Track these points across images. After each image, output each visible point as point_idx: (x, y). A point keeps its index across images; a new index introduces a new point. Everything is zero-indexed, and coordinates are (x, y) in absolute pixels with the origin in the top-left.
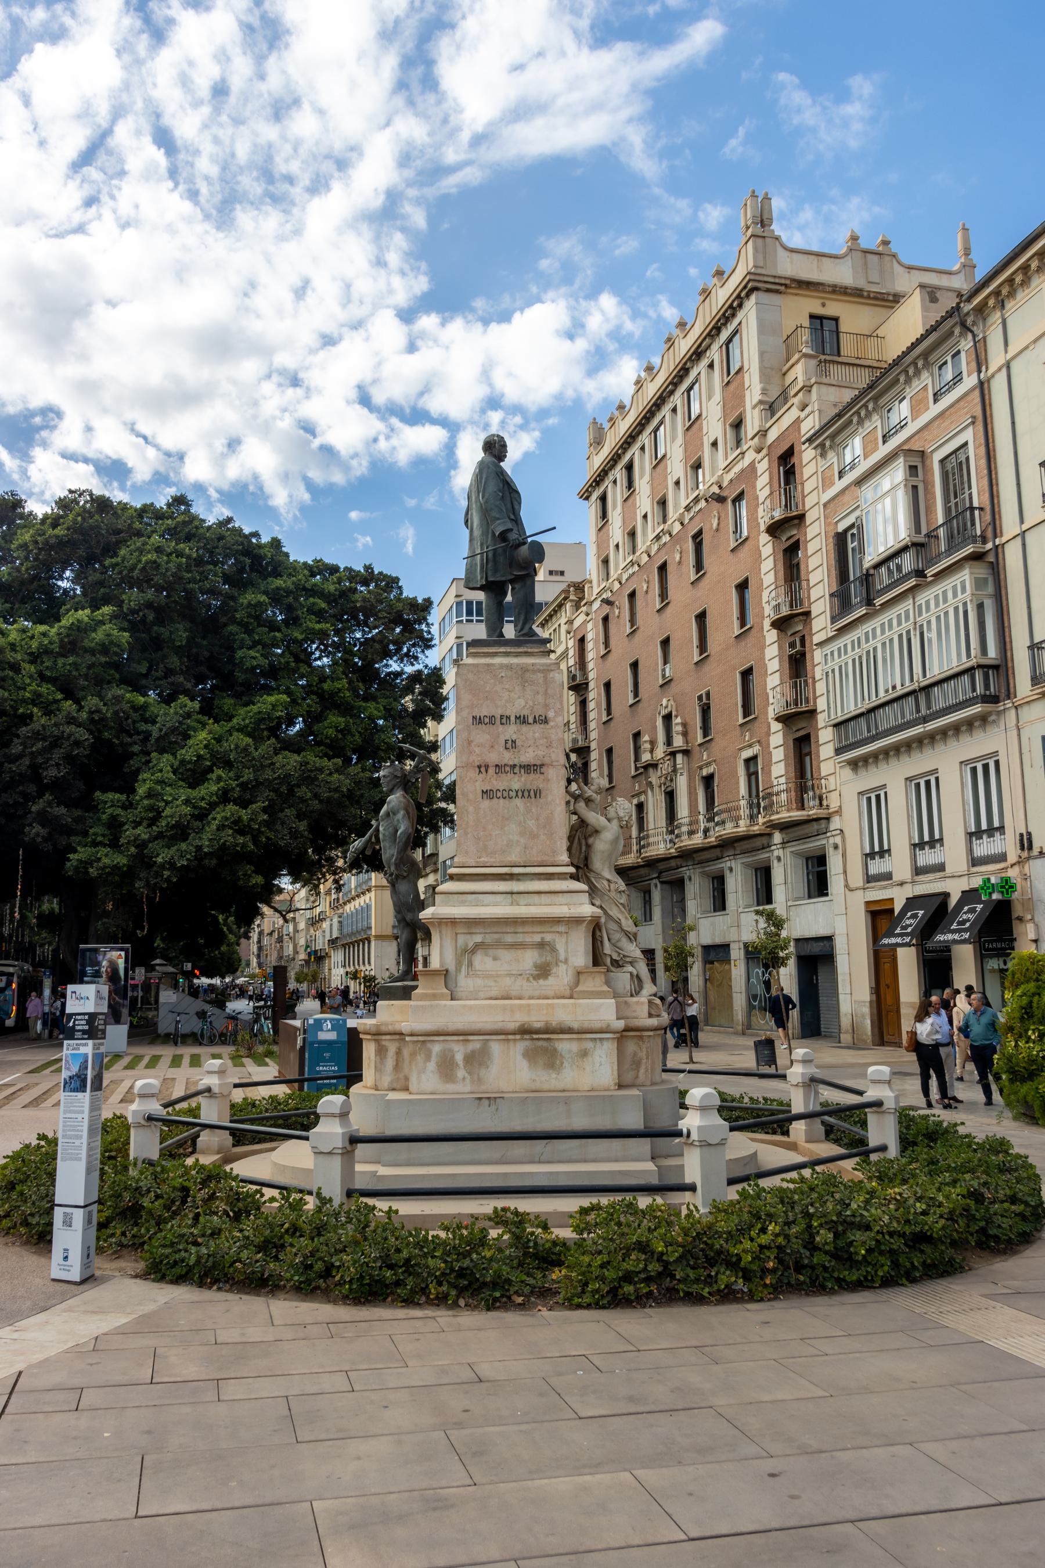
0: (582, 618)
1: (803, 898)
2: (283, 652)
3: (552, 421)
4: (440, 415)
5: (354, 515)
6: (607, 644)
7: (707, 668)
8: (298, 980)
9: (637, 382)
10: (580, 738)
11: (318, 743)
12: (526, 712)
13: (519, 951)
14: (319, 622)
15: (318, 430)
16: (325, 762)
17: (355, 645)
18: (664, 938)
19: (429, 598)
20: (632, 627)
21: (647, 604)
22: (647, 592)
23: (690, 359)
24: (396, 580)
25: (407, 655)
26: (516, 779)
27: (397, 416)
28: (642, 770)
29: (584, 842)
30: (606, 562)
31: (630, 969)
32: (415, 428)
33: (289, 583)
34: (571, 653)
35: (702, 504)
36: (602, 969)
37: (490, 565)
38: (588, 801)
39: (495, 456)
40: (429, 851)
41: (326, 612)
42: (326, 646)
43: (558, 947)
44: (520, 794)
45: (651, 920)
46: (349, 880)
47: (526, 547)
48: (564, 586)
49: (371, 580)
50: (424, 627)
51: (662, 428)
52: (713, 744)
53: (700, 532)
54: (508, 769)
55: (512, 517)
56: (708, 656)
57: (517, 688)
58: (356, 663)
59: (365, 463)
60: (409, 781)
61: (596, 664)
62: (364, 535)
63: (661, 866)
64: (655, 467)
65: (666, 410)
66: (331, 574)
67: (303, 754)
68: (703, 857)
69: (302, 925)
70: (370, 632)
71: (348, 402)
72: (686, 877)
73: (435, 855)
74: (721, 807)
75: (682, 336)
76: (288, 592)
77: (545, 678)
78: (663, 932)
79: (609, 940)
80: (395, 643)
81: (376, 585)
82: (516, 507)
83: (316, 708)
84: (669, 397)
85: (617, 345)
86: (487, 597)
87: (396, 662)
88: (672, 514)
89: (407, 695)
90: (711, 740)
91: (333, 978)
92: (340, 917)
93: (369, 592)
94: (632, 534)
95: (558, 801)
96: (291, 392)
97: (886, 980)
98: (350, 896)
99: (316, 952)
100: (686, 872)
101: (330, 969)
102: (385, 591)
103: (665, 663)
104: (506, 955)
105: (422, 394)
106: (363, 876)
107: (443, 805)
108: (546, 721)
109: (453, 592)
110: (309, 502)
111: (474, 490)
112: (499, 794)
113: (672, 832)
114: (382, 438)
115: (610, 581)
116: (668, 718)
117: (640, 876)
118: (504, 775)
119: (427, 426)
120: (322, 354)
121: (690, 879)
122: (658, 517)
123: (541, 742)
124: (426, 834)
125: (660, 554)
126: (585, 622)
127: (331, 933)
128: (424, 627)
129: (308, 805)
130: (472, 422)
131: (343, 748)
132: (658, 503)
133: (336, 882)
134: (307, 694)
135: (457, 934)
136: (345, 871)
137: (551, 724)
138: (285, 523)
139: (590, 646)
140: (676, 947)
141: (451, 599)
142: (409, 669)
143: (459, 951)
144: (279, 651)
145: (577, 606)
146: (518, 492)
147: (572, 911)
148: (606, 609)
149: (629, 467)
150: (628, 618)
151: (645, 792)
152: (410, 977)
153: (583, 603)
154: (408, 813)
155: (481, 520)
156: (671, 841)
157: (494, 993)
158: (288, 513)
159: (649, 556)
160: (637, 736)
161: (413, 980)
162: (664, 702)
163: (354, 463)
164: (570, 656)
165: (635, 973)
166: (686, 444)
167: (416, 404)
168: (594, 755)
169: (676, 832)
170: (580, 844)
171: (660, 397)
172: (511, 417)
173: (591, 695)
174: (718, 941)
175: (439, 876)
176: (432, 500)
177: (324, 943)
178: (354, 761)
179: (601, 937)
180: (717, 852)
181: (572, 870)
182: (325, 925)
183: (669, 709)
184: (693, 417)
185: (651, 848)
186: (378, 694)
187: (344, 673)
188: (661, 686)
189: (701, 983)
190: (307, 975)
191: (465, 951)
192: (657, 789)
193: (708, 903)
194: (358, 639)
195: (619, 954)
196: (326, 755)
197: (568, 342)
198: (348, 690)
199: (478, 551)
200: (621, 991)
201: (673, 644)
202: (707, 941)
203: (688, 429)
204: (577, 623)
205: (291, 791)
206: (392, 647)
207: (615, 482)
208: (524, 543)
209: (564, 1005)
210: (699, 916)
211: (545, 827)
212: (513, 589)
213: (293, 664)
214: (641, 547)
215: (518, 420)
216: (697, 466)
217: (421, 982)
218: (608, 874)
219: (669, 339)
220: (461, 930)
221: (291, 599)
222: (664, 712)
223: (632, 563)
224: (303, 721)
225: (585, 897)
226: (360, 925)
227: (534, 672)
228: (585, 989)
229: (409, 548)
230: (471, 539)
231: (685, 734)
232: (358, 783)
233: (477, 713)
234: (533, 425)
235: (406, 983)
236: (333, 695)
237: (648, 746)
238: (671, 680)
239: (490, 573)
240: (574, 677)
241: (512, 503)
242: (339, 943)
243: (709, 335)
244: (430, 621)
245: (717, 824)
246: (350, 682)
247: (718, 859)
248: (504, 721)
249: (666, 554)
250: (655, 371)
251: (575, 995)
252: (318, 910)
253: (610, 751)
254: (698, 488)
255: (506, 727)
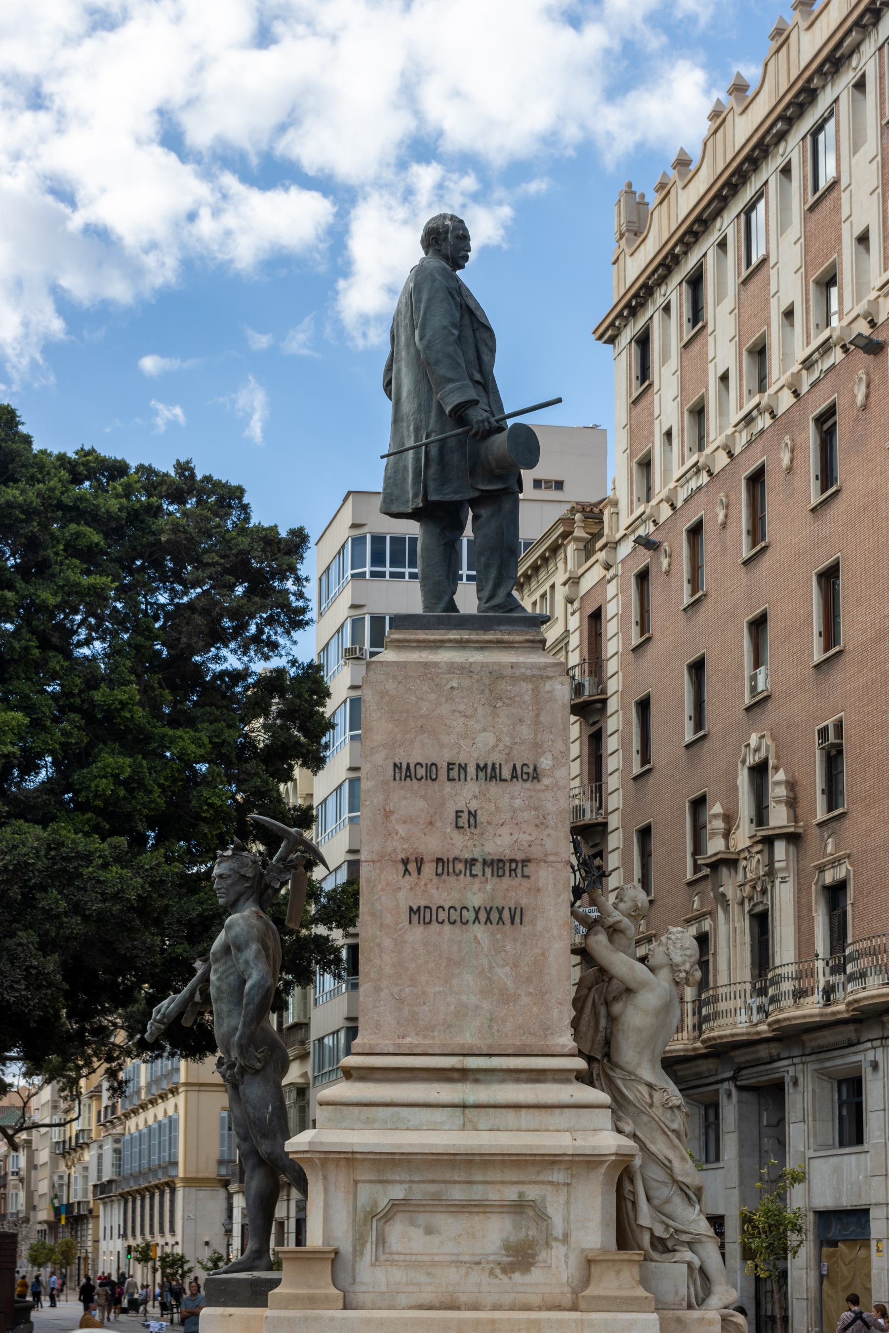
0: (596, 573)
1: (833, 1147)
2: (18, 629)
3: (536, 187)
4: (321, 169)
5: (149, 364)
6: (644, 624)
7: (838, 675)
8: (35, 1261)
9: (715, 115)
10: (587, 806)
11: (81, 807)
12: (496, 758)
13: (476, 1218)
14: (88, 572)
15: (80, 196)
16: (96, 843)
17: (156, 618)
18: (742, 1195)
19: (301, 529)
20: (694, 592)
21: (724, 550)
22: (724, 525)
23: (819, 70)
24: (239, 492)
25: (256, 639)
26: (476, 887)
27: (234, 171)
28: (706, 871)
29: (603, 1011)
30: (646, 464)
31: (688, 1255)
32: (271, 195)
33: (31, 494)
34: (574, 640)
35: (837, 355)
36: (634, 1255)
37: (432, 471)
38: (613, 931)
39: (446, 258)
40: (290, 1018)
41: (103, 552)
42: (100, 619)
43: (550, 1211)
44: (483, 916)
45: (717, 1159)
46: (137, 1069)
47: (501, 438)
48: (562, 511)
49: (190, 492)
50: (290, 585)
51: (761, 205)
52: (847, 822)
53: (831, 411)
54: (460, 866)
55: (478, 377)
56: (840, 652)
57: (480, 711)
58: (160, 652)
59: (171, 262)
60: (268, 886)
61: (623, 665)
62: (170, 402)
63: (741, 1056)
64: (745, 282)
65: (769, 170)
66: (112, 478)
67: (53, 826)
68: (822, 1042)
69: (43, 1156)
70: (185, 593)
71: (139, 142)
72: (787, 1079)
73: (302, 1026)
74: (857, 946)
75: (804, 25)
76: (29, 512)
77: (536, 691)
78: (741, 1183)
79: (648, 1199)
80: (234, 614)
81: (199, 502)
82: (486, 358)
83: (80, 738)
84: (777, 144)
85: (664, 39)
86: (426, 532)
87: (234, 651)
88: (777, 375)
89: (256, 716)
90: (843, 815)
91: (102, 1258)
92: (117, 1141)
93: (185, 514)
94: (698, 412)
95: (555, 931)
96: (28, 120)
97: (394, 1075)
98: (137, 1102)
99: (70, 1206)
100: (787, 1069)
101: (96, 1241)
102: (216, 514)
103: (757, 664)
104: (449, 1225)
105: (282, 128)
106: (164, 1064)
107: (320, 930)
108: (535, 776)
109: (347, 517)
110: (61, 336)
111: (404, 322)
112: (443, 915)
113: (762, 992)
114: (205, 213)
115: (654, 502)
116: (759, 771)
117: (699, 1076)
118: (452, 879)
119: (294, 191)
120: (89, 46)
121: (795, 1083)
122: (750, 381)
123: (526, 815)
124: (288, 985)
125: (751, 451)
126: (603, 582)
127: (100, 1171)
128: (290, 585)
129: (61, 926)
130: (380, 185)
131: (129, 816)
132: (750, 352)
133: (112, 1074)
134: (62, 710)
135: (356, 1182)
136: (128, 1053)
137: (546, 781)
138: (15, 376)
139: (611, 628)
140: (767, 1213)
141: (341, 533)
142: (260, 667)
143: (361, 1215)
144: (9, 626)
145: (588, 550)
146: (488, 329)
147: (580, 1142)
148: (645, 557)
149: (696, 281)
150: (686, 576)
151: (711, 914)
152: (263, 1263)
153: (599, 545)
154: (265, 947)
155: (417, 383)
156: (760, 1009)
157: (426, 1297)
158: (20, 355)
159: (730, 455)
160: (699, 804)
161: (270, 1268)
162: (754, 740)
163: (150, 261)
164: (571, 647)
165: (697, 1263)
166: (808, 239)
167: (272, 148)
168: (614, 841)
169: (771, 992)
170: (596, 1015)
171: (760, 145)
172: (455, 176)
173: (612, 724)
174: (846, 1202)
175: (309, 1067)
176: (301, 337)
177: (85, 1190)
178: (151, 842)
179: (634, 1193)
180: (849, 1032)
181: (580, 1064)
182: (89, 1156)
183: (763, 754)
184: (823, 185)
185: (721, 1021)
186: (199, 712)
187: (132, 671)
188: (748, 709)
189: (813, 1282)
190: (52, 1250)
191: (372, 1215)
192: (735, 909)
193: (830, 1130)
194: (163, 606)
195: (668, 1226)
196: (97, 829)
197: (569, 33)
198: (141, 704)
199: (410, 443)
200: (670, 1298)
201: (773, 629)
202: (825, 1200)
203: (812, 209)
204: (586, 584)
205: (29, 900)
206: (227, 623)
207: (667, 309)
208: (501, 429)
209: (560, 1322)
210: (811, 1153)
211: (529, 980)
212: (476, 518)
213: (36, 652)
214: (715, 437)
215: (469, 183)
216: (829, 281)
217: (284, 1274)
218: (649, 1072)
219: (779, 32)
220: (364, 1175)
221: (34, 526)
222: (751, 760)
223: (697, 469)
224: (53, 763)
225: (605, 1118)
226: (155, 1158)
227: (515, 679)
228: (603, 1293)
229: (256, 428)
230: (397, 419)
231: (792, 803)
232: (158, 884)
233: (402, 757)
234: (499, 193)
235: (257, 1274)
236: (110, 714)
237: (719, 824)
238: (767, 698)
239: (431, 485)
240: (578, 689)
241: (477, 350)
242: (115, 1191)
243: (857, 24)
244: (302, 573)
245: (851, 978)
246: (145, 690)
247: (851, 1045)
248: (454, 774)
249: (764, 452)
250: (750, 93)
251: (582, 1305)
252: (76, 1127)
253: (645, 833)
254: (828, 324)
255: (458, 785)
